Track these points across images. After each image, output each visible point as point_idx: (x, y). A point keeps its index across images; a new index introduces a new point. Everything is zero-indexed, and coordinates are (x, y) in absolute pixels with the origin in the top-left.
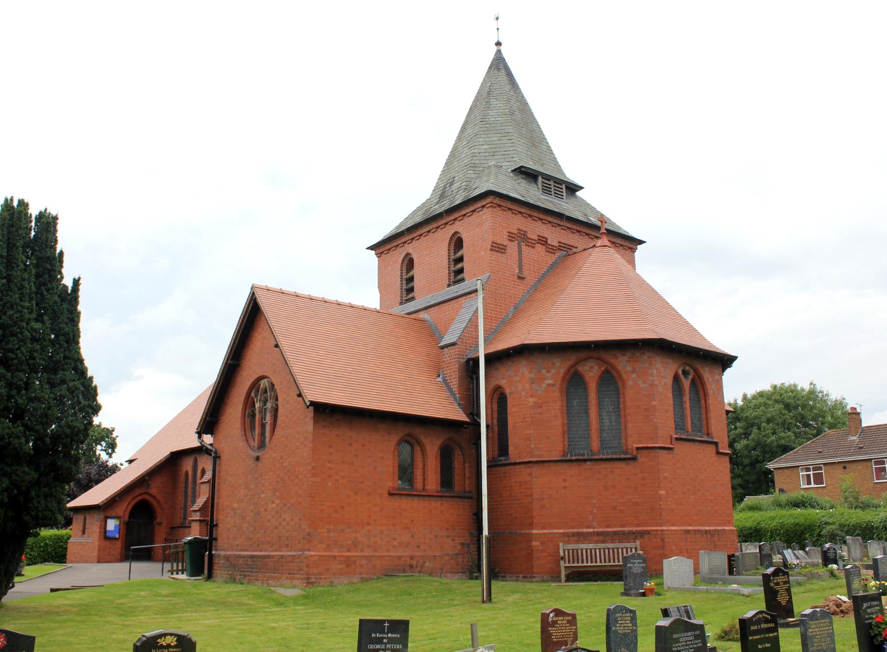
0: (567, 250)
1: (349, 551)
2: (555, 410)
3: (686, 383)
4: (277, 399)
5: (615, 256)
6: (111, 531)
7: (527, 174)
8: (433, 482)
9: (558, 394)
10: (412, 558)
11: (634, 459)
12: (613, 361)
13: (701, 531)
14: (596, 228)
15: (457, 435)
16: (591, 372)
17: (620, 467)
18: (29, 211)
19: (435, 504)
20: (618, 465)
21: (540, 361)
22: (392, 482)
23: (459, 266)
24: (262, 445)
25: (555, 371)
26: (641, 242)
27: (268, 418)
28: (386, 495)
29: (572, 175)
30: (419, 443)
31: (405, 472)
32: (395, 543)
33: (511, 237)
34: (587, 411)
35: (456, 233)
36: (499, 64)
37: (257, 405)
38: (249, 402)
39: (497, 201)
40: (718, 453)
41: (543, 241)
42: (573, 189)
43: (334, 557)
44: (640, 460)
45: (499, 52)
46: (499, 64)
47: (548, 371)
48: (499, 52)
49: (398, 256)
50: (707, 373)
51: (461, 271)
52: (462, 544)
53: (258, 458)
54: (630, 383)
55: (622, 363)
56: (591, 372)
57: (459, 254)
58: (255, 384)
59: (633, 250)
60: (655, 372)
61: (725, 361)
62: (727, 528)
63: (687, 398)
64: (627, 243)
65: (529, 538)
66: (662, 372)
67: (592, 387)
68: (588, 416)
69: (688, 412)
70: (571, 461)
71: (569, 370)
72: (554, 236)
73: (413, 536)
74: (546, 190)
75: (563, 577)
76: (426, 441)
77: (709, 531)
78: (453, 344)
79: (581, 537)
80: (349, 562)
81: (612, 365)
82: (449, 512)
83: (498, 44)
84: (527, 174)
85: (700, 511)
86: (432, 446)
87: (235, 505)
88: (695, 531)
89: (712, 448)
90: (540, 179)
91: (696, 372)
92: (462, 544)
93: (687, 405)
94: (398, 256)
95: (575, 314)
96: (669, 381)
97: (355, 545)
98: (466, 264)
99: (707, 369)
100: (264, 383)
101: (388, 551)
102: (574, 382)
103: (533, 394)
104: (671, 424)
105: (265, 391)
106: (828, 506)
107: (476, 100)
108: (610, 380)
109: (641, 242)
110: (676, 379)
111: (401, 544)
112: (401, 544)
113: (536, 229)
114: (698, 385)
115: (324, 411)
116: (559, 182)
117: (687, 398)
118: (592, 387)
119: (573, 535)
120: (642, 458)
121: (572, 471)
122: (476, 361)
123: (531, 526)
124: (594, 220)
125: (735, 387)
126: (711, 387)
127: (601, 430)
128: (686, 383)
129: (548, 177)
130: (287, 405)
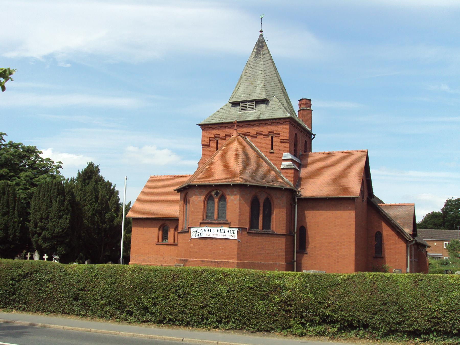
6: (172, 228)
12: (224, 192)
13: (212, 262)
18: (121, 202)
32: (157, 260)
45: (261, 36)
48: (261, 36)
49: (212, 133)
62: (230, 261)
73: (163, 258)
77: (217, 262)
83: (261, 31)
85: (214, 253)
88: (208, 261)
97: (144, 260)
101: (154, 263)
106: (9, 268)
108: (223, 198)
111: (159, 261)
112: (159, 261)
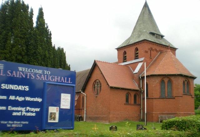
0: (161, 52)
1: (117, 116)
2: (158, 88)
3: (186, 83)
4: (101, 84)
5: (170, 53)
7: (153, 34)
8: (133, 102)
9: (159, 84)
10: (129, 117)
11: (174, 98)
12: (171, 78)
14: (167, 46)
15: (138, 93)
16: (166, 80)
17: (171, 100)
19: (133, 107)
20: (171, 99)
21: (123, 91)
22: (125, 102)
23: (137, 55)
24: (97, 94)
25: (158, 80)
26: (177, 49)
27: (99, 89)
28: (124, 105)
29: (162, 32)
30: (130, 94)
31: (127, 100)
33: (149, 49)
34: (165, 88)
35: (137, 47)
36: (146, 6)
37: (96, 85)
38: (94, 85)
39: (146, 41)
40: (192, 97)
41: (156, 50)
42: (162, 36)
43: (114, 117)
44: (176, 98)
46: (146, 6)
47: (157, 80)
50: (190, 80)
51: (138, 56)
52: (138, 115)
53: (96, 97)
54: (174, 82)
55: (172, 78)
56: (166, 80)
57: (137, 52)
58: (95, 81)
59: (175, 50)
60: (179, 80)
61: (194, 78)
63: (186, 86)
64: (174, 49)
65: (152, 114)
66: (181, 80)
67: (166, 83)
68: (165, 89)
69: (186, 89)
70: (161, 98)
71: (161, 80)
72: (158, 48)
74: (157, 37)
75: (159, 122)
76: (131, 94)
78: (137, 73)
79: (163, 114)
80: (117, 118)
81: (170, 79)
82: (136, 108)
84: (153, 34)
86: (133, 94)
87: (91, 106)
89: (190, 96)
90: (155, 35)
91: (188, 80)
92: (138, 115)
93: (186, 87)
94: (122, 51)
95: (163, 67)
96: (182, 82)
98: (139, 55)
99: (191, 80)
100: (97, 81)
102: (162, 82)
103: (156, 82)
104: (183, 91)
105: (98, 82)
107: (140, 14)
108: (170, 81)
109: (177, 49)
110: (184, 82)
113: (154, 47)
114: (188, 83)
115: (112, 88)
116: (159, 35)
117: (186, 86)
118: (166, 83)
119: (162, 113)
120: (176, 98)
121: (162, 100)
122: (144, 77)
123: (153, 111)
124: (168, 45)
125: (196, 82)
126: (191, 83)
127: (168, 92)
128: (186, 83)
129: (157, 34)
130: (104, 86)
